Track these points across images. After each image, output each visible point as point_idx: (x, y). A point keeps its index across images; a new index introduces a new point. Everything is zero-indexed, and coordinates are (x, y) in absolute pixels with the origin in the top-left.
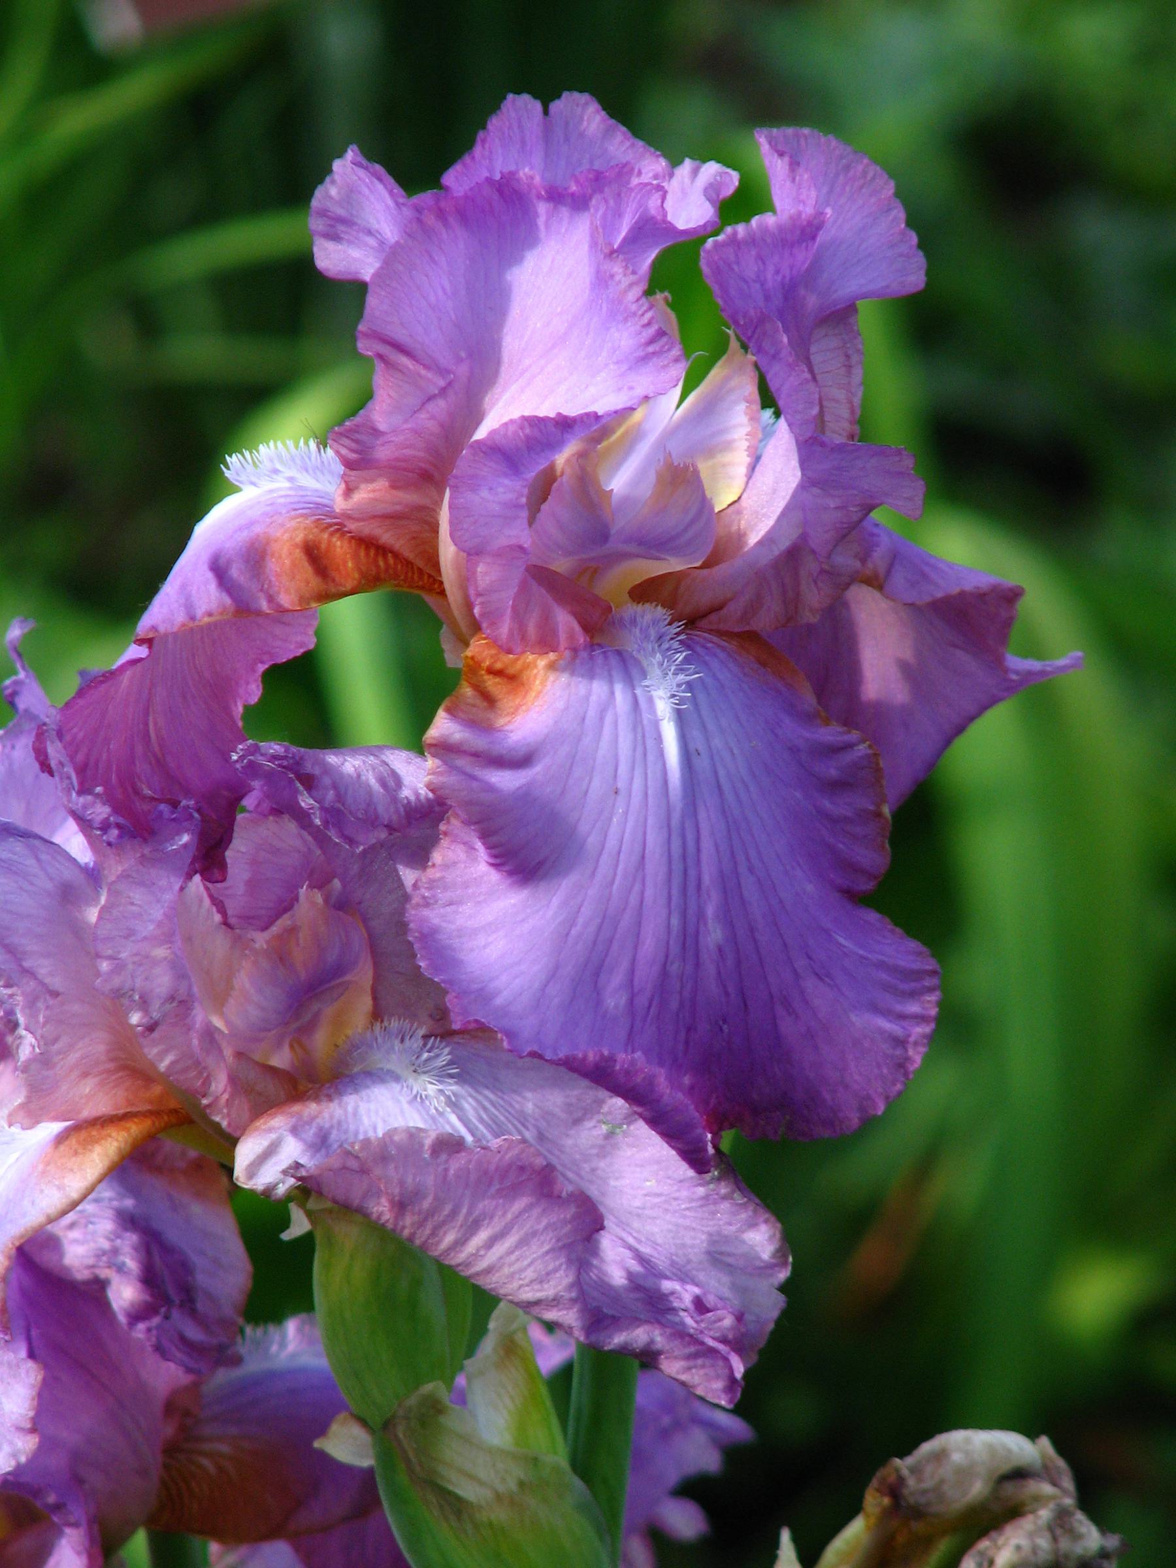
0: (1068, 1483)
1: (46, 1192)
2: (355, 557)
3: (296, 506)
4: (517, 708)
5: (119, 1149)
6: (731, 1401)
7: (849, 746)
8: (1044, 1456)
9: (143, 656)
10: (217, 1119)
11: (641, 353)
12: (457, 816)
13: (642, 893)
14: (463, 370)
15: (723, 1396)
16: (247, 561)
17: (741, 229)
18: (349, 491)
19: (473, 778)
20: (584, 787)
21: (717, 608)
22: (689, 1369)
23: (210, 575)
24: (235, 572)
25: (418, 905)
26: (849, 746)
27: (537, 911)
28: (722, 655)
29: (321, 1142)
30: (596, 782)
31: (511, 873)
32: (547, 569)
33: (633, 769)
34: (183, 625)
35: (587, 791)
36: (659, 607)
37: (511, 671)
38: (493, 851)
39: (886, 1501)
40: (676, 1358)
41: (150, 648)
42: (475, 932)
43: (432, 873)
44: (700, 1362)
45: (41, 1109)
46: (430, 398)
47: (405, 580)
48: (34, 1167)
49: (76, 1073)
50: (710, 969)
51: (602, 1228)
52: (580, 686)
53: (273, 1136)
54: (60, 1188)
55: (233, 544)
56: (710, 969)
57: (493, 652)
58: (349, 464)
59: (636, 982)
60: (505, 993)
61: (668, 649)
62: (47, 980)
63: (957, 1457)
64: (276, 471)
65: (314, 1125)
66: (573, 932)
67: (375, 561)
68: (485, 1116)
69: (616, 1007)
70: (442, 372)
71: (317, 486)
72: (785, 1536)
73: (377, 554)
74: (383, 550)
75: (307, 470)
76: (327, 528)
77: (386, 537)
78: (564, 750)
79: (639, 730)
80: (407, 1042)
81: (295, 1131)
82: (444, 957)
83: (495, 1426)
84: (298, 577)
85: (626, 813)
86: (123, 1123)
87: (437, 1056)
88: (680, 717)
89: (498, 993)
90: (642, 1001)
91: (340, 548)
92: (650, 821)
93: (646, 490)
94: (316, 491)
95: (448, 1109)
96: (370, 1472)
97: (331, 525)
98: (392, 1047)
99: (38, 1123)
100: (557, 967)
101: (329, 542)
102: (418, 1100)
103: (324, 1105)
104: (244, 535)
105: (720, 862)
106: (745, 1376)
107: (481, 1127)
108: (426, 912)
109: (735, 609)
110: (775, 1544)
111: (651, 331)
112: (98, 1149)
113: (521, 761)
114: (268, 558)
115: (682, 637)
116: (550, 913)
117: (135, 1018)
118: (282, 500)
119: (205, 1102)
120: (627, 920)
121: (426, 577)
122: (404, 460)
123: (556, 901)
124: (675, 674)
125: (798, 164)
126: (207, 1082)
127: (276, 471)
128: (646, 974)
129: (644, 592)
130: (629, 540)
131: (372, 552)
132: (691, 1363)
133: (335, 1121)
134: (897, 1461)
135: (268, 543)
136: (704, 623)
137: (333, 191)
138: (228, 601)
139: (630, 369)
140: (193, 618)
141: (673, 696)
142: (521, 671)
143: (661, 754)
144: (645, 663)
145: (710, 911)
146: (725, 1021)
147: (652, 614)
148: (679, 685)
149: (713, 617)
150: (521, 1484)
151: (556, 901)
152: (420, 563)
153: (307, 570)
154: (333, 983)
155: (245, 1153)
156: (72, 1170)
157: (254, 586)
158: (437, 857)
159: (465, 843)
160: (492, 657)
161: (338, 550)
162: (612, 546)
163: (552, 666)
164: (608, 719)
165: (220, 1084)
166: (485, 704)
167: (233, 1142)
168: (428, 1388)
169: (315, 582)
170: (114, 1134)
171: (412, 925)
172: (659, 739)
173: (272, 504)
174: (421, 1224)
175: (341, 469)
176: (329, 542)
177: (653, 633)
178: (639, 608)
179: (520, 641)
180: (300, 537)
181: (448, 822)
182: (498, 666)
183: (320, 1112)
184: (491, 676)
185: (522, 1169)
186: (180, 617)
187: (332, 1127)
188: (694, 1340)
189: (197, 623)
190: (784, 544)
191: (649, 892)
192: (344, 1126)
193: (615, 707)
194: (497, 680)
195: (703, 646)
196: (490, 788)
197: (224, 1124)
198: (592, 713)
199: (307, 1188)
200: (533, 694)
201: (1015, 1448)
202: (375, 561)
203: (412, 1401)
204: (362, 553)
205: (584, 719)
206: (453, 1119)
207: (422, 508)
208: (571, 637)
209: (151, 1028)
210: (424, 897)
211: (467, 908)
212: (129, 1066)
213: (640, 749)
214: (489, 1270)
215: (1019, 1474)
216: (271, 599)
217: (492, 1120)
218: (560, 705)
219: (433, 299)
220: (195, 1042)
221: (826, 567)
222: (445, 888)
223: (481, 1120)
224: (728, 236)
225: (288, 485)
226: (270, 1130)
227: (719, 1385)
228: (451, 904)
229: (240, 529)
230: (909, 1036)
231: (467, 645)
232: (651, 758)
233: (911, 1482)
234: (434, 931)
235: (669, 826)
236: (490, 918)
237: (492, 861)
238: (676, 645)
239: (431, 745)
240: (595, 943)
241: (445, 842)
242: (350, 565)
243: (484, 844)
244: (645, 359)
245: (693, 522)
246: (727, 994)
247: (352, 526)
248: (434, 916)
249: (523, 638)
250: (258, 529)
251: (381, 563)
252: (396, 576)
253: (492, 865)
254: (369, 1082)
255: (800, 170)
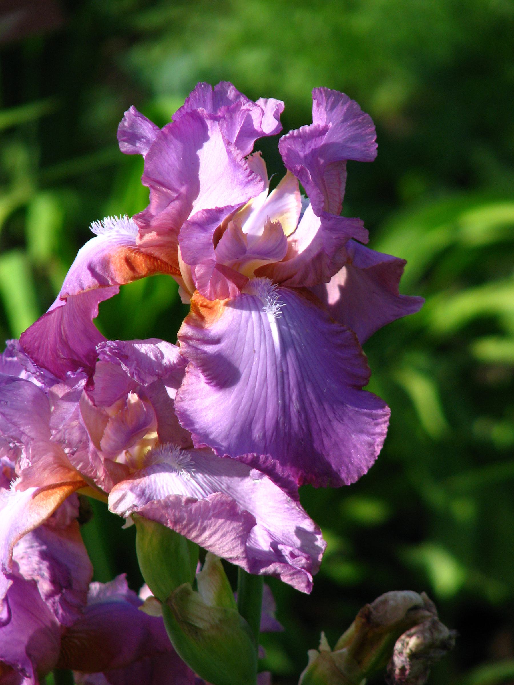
0: (435, 611)
1: (32, 515)
2: (145, 262)
3: (121, 242)
4: (213, 320)
5: (61, 498)
6: (309, 591)
7: (343, 331)
8: (424, 600)
9: (63, 305)
10: (100, 486)
11: (247, 180)
12: (192, 364)
13: (267, 391)
14: (183, 190)
15: (306, 589)
16: (102, 265)
17: (296, 131)
18: (142, 237)
19: (197, 349)
20: (242, 350)
21: (291, 277)
22: (292, 579)
23: (88, 272)
24: (98, 270)
25: (179, 401)
26: (343, 331)
27: (226, 400)
28: (293, 297)
29: (142, 494)
30: (246, 348)
31: (215, 386)
32: (222, 265)
33: (260, 343)
34: (79, 292)
35: (243, 353)
36: (267, 279)
37: (210, 305)
38: (209, 377)
39: (363, 620)
40: (286, 575)
41: (66, 301)
42: (201, 410)
43: (183, 388)
44: (295, 576)
45: (28, 484)
46: (173, 200)
47: (165, 270)
48: (26, 505)
49: (41, 469)
50: (295, 420)
51: (256, 524)
52: (238, 312)
53: (123, 492)
54: (38, 514)
55: (96, 259)
56: (295, 420)
57: (203, 298)
58: (141, 227)
59: (266, 427)
60: (215, 433)
61: (272, 295)
62: (29, 434)
63: (392, 602)
64: (111, 228)
65: (139, 487)
66: (240, 408)
67: (153, 263)
68: (206, 481)
69: (259, 437)
70: (176, 191)
71: (127, 233)
72: (323, 635)
73: (154, 261)
74: (156, 259)
75: (123, 228)
76: (133, 251)
77: (156, 254)
78: (233, 337)
79: (262, 327)
80: (174, 452)
81: (132, 490)
82: (190, 422)
83: (209, 596)
84: (123, 271)
85: (259, 360)
86: (61, 487)
87: (186, 457)
88: (278, 321)
89: (211, 433)
90: (269, 434)
91: (140, 261)
92: (268, 363)
93: (260, 233)
94: (128, 236)
95: (191, 478)
96: (161, 619)
97: (135, 250)
98: (168, 454)
99: (27, 489)
100: (234, 423)
101: (135, 257)
102: (186, 484)
103: (142, 478)
104: (101, 255)
105: (297, 377)
106: (313, 581)
107: (205, 485)
108: (182, 404)
109: (297, 278)
110: (319, 638)
111: (248, 171)
112: (52, 498)
113: (216, 341)
114: (111, 263)
115: (277, 290)
116: (231, 401)
117: (67, 451)
118: (115, 240)
119: (95, 480)
120: (261, 402)
121: (173, 269)
122: (163, 224)
123: (233, 396)
124: (276, 305)
125: (320, 104)
126: (96, 472)
127: (111, 228)
128: (270, 423)
129: (261, 272)
130: (254, 253)
131: (152, 260)
132: (293, 577)
133: (147, 485)
134: (368, 605)
135: (110, 258)
136: (284, 284)
137: (126, 124)
138: (96, 281)
139: (245, 186)
140: (83, 289)
141: (275, 313)
142: (214, 305)
143: (271, 336)
144: (263, 301)
145: (294, 397)
146: (302, 440)
147: (264, 281)
148: (277, 309)
149: (288, 281)
150: (220, 621)
151: (233, 396)
152: (170, 263)
153: (126, 268)
154: (144, 429)
155: (112, 499)
156: (42, 507)
157: (105, 275)
158: (185, 381)
159: (195, 375)
160: (202, 300)
161: (138, 260)
162: (248, 254)
163: (227, 304)
164: (250, 324)
165: (101, 473)
166: (201, 319)
167: (107, 495)
168: (184, 585)
169: (130, 273)
170: (58, 492)
171: (176, 409)
172: (270, 330)
173: (110, 242)
174: (183, 529)
175: (138, 229)
176: (135, 257)
177: (266, 289)
178: (260, 279)
179: (214, 295)
180: (123, 256)
181: (189, 367)
182: (205, 304)
183: (141, 482)
184: (202, 308)
185: (222, 504)
186: (78, 290)
187: (146, 487)
188: (292, 567)
189: (84, 291)
190: (315, 252)
191: (269, 391)
192: (151, 487)
193: (252, 318)
194: (205, 309)
195: (285, 293)
196: (205, 353)
197: (103, 488)
198: (243, 321)
199: (140, 516)
200: (220, 315)
201: (414, 598)
202: (153, 263)
203: (177, 590)
204: (148, 261)
205: (240, 324)
206: (194, 482)
207: (171, 242)
208: (234, 291)
209: (73, 453)
210: (181, 398)
211: (198, 401)
212: (61, 464)
213: (263, 334)
214: (211, 546)
215: (416, 608)
216: (112, 280)
217: (209, 481)
218: (230, 318)
219: (170, 162)
220: (90, 457)
221: (332, 261)
222: (189, 394)
223: (204, 482)
224: (290, 135)
225: (116, 233)
226: (122, 490)
227: (303, 585)
228: (191, 400)
229: (99, 252)
230: (375, 442)
231: (191, 296)
232: (267, 337)
233: (374, 613)
234: (185, 411)
235: (276, 364)
236: (207, 404)
237: (207, 381)
238: (275, 293)
239: (180, 337)
240: (249, 412)
241: (187, 376)
242: (143, 265)
243: (203, 375)
244: (249, 182)
245: (279, 245)
246: (303, 429)
247: (143, 250)
248: (185, 405)
249: (216, 293)
250: (106, 252)
251: (156, 264)
252: (162, 269)
253: (207, 383)
254: (159, 468)
255: (321, 106)
